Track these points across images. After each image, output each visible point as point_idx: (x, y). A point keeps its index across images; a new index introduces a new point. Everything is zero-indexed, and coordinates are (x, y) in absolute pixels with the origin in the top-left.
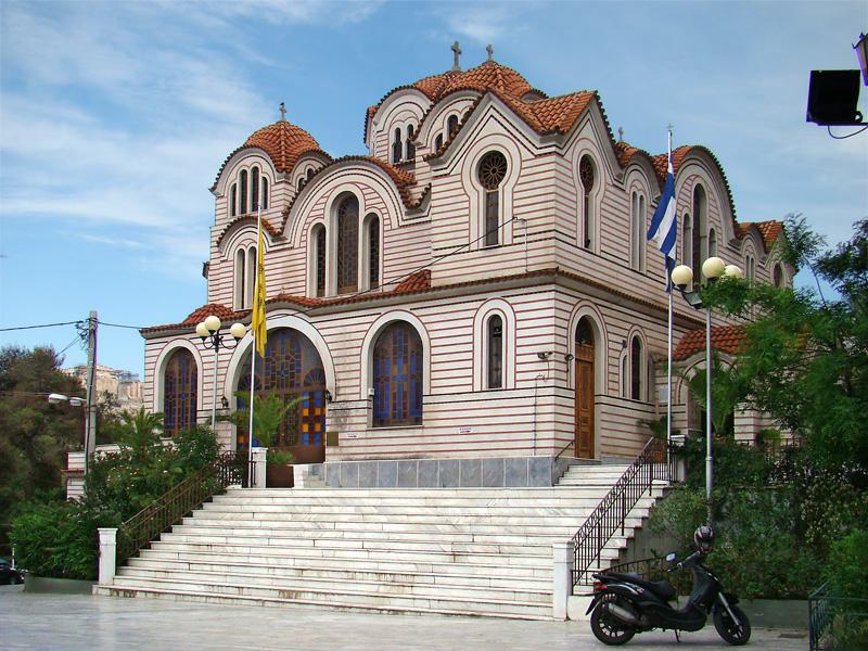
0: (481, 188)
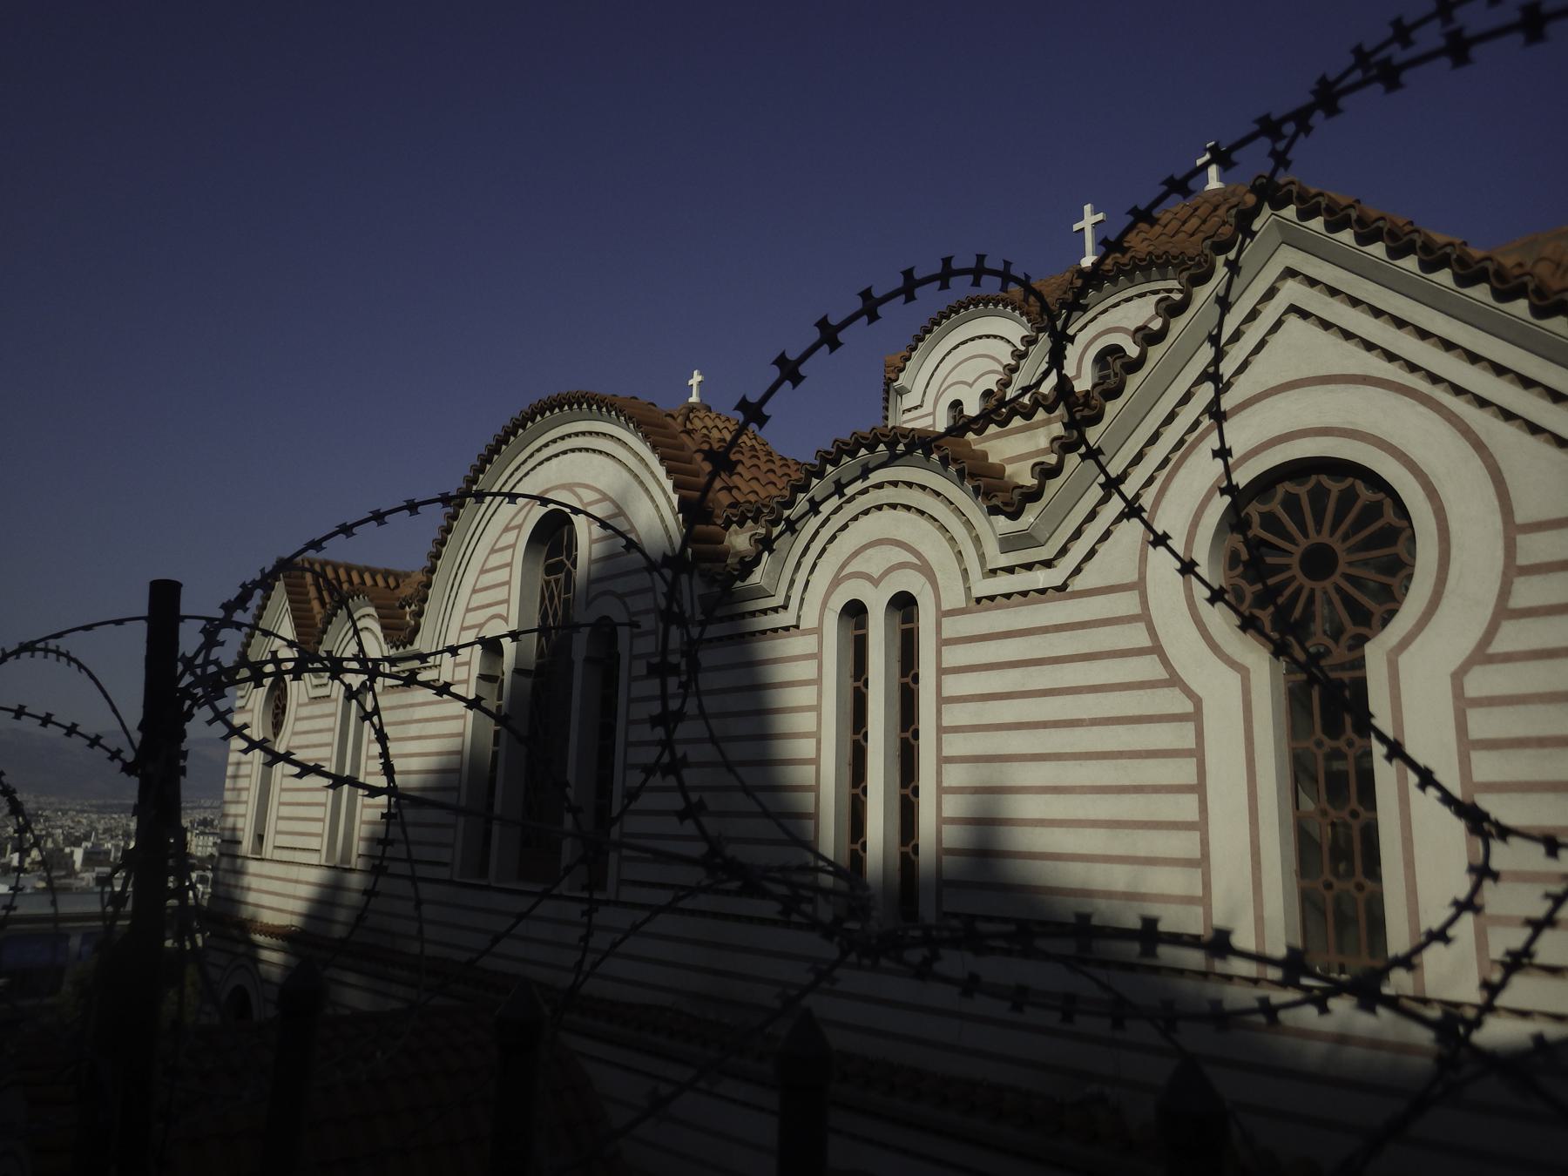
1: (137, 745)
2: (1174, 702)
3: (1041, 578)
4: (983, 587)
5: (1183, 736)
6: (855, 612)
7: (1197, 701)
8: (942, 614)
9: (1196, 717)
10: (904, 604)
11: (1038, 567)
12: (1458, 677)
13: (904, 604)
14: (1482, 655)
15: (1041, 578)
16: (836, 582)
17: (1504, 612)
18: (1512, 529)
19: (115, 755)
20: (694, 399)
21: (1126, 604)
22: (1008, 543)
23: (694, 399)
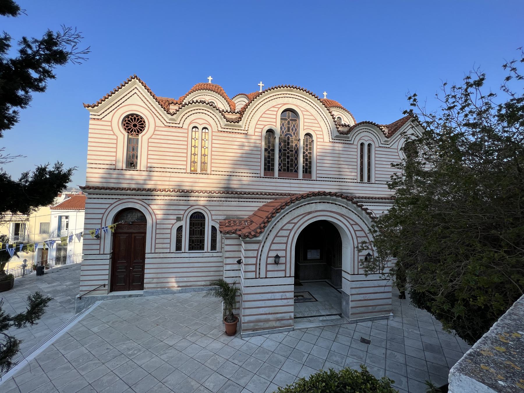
0: (126, 134)
1: (343, 272)
2: (115, 137)
3: (387, 146)
4: (220, 129)
5: (115, 141)
6: (362, 144)
7: (117, 137)
8: (375, 147)
9: (117, 139)
10: (369, 145)
11: (385, 146)
12: (148, 139)
13: (369, 145)
14: (150, 138)
15: (387, 146)
16: (360, 139)
17: (153, 134)
18: (155, 126)
19: (385, 134)
20: (325, 98)
21: (109, 124)
22: (226, 125)
23: (325, 98)
